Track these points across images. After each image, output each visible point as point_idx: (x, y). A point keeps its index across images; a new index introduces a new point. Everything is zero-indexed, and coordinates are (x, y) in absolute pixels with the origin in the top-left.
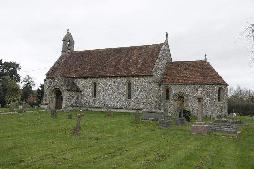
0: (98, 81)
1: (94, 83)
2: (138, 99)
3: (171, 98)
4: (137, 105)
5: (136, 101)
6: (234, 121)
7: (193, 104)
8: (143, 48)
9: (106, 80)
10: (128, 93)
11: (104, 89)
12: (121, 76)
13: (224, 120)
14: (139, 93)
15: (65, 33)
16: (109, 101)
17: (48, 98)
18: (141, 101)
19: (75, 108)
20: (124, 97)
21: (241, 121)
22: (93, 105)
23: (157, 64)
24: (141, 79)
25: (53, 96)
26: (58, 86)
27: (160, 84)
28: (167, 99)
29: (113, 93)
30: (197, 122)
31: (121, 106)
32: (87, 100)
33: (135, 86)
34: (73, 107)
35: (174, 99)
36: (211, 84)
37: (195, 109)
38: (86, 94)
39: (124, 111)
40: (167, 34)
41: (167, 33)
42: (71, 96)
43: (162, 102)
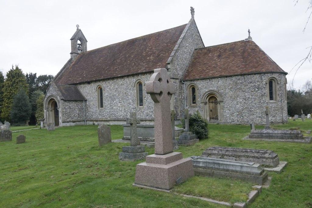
0: (103, 84)
3: (198, 100)
6: (286, 134)
8: (162, 34)
9: (113, 83)
10: (139, 98)
11: (111, 95)
12: (128, 74)
13: (268, 133)
15: (74, 31)
16: (117, 111)
19: (77, 122)
21: (298, 134)
23: (175, 51)
25: (50, 110)
27: (182, 82)
28: (194, 102)
29: (121, 99)
30: (153, 156)
32: (93, 112)
34: (73, 122)
35: (203, 101)
36: (257, 73)
37: (233, 114)
38: (91, 103)
40: (192, 10)
41: (191, 7)
42: (70, 108)
43: (187, 107)
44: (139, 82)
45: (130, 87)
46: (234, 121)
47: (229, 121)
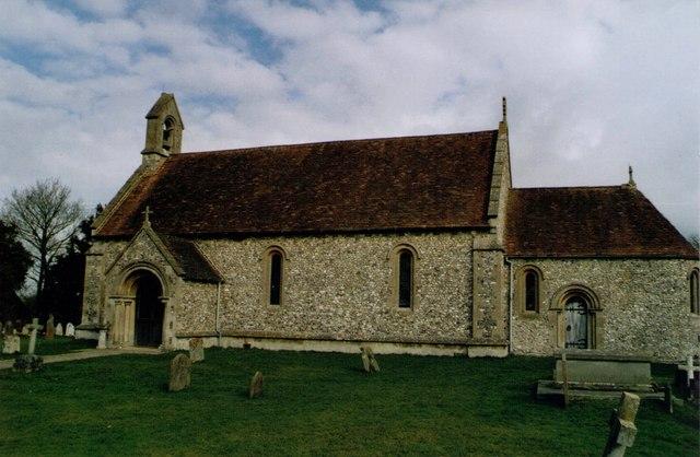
5: (428, 313)
22: (268, 329)
26: (148, 263)
31: (373, 331)
38: (242, 291)
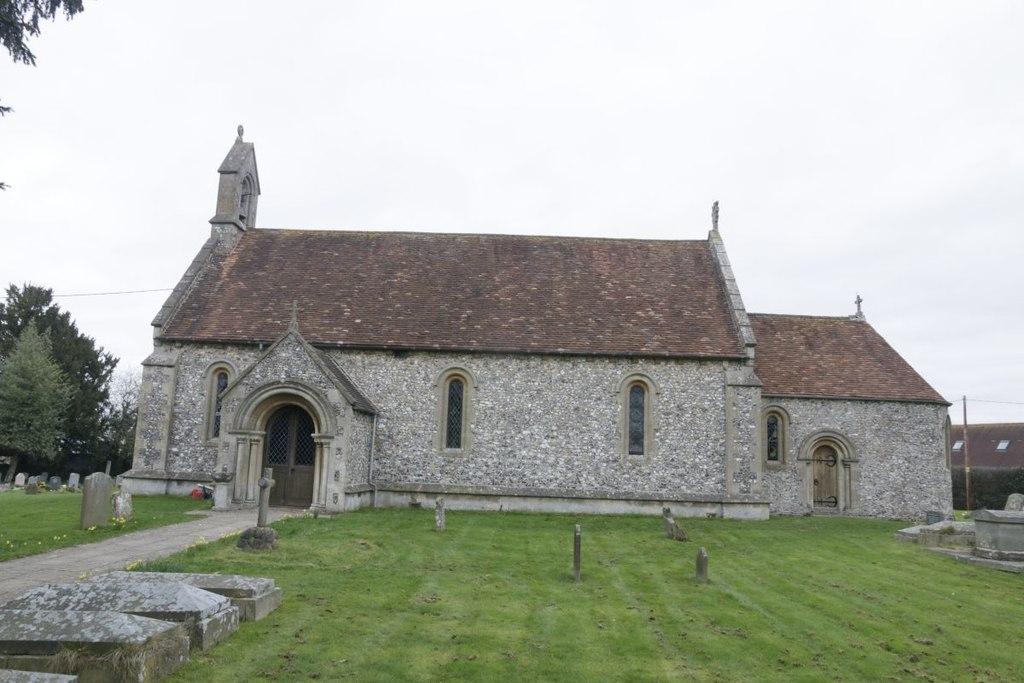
0: (475, 368)
1: (218, 373)
2: (680, 458)
4: (678, 481)
5: (669, 463)
7: (875, 475)
14: (684, 430)
17: (227, 445)
18: (695, 466)
20: (613, 445)
22: (445, 481)
24: (692, 371)
26: (295, 383)
29: (554, 428)
31: (597, 485)
32: (408, 460)
33: (666, 399)
37: (882, 493)
39: (621, 508)
44: (221, 369)
45: (598, 391)
46: (883, 513)
47: (872, 510)
